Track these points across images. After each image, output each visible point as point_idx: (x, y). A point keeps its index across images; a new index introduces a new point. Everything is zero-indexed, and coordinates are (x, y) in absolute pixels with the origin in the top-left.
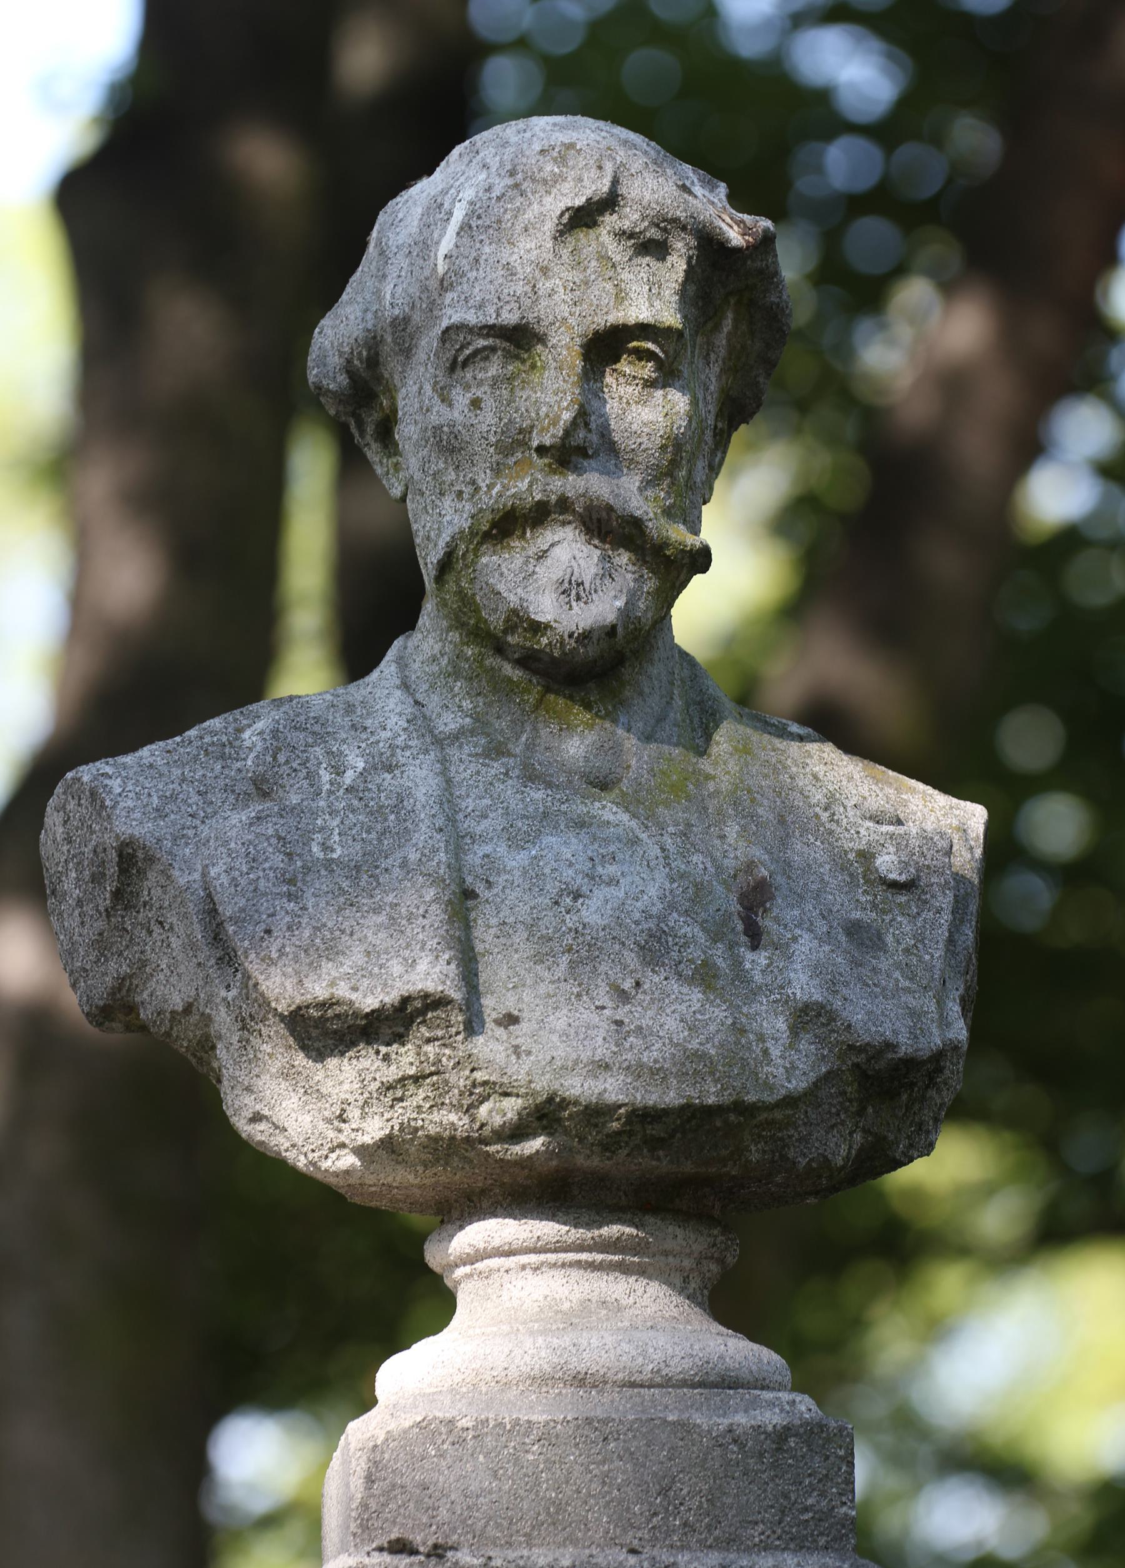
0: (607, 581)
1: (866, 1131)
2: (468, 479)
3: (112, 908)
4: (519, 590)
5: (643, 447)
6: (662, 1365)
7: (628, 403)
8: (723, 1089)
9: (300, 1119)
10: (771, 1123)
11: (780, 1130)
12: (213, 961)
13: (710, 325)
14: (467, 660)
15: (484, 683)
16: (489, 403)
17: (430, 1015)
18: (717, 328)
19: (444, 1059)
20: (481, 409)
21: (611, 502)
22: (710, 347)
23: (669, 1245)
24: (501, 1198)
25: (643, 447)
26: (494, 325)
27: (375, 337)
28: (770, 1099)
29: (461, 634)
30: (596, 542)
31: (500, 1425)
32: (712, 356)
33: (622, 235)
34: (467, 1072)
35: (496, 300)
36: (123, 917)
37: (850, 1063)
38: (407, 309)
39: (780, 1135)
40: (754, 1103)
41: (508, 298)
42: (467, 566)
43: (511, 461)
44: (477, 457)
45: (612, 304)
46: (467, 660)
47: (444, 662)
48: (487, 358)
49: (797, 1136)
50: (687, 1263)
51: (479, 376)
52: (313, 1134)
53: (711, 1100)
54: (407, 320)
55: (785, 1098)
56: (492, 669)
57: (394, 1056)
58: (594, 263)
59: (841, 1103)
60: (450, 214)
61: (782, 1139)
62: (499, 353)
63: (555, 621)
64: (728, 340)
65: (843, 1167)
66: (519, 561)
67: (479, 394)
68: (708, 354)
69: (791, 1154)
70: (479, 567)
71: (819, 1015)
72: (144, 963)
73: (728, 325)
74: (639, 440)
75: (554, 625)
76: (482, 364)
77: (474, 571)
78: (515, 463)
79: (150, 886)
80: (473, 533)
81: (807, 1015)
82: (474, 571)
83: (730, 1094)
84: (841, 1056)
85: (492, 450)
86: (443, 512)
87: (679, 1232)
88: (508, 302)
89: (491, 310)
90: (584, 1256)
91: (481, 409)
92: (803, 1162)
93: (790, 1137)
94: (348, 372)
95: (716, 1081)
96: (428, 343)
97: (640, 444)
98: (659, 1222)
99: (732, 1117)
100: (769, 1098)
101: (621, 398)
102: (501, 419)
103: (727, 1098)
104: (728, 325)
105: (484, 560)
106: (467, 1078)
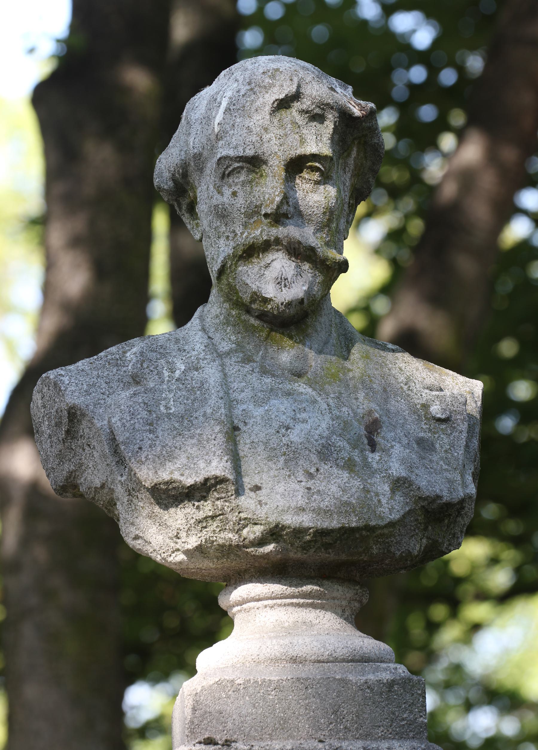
0: (299, 277)
1: (428, 538)
2: (231, 230)
3: (65, 438)
4: (257, 283)
5: (315, 213)
6: (333, 652)
7: (307, 192)
8: (359, 519)
9: (157, 538)
10: (382, 535)
11: (387, 538)
12: (114, 463)
13: (345, 154)
14: (233, 316)
15: (241, 327)
16: (241, 194)
17: (218, 487)
18: (349, 155)
19: (226, 508)
20: (237, 196)
21: (300, 240)
22: (346, 165)
23: (335, 594)
24: (254, 574)
25: (315, 213)
26: (242, 156)
27: (185, 163)
28: (382, 524)
29: (230, 304)
30: (293, 259)
31: (256, 682)
32: (347, 169)
33: (302, 112)
34: (237, 514)
35: (243, 144)
36: (71, 443)
37: (420, 505)
38: (200, 149)
39: (387, 540)
40: (374, 526)
41: (249, 143)
42: (232, 272)
43: (252, 221)
44: (235, 220)
45: (298, 145)
46: (233, 316)
47: (222, 317)
48: (239, 172)
49: (395, 541)
50: (344, 603)
51: (236, 181)
52: (164, 544)
53: (354, 525)
54: (200, 154)
55: (389, 523)
56: (245, 320)
57: (201, 507)
58: (289, 126)
59: (416, 525)
60: (220, 103)
61: (388, 543)
62: (245, 169)
63: (275, 297)
64: (355, 161)
65: (417, 556)
66: (256, 269)
67: (236, 189)
68: (345, 168)
69: (393, 549)
70: (237, 272)
71: (405, 483)
72: (81, 465)
73: (354, 154)
74: (313, 210)
75: (274, 299)
76: (237, 175)
77: (235, 274)
78: (254, 222)
79: (84, 428)
80: (234, 256)
81: (399, 483)
82: (235, 274)
83: (363, 522)
84: (416, 502)
85: (242, 216)
86: (220, 246)
87: (340, 588)
88: (249, 145)
89: (241, 149)
90: (295, 601)
91: (237, 196)
92: (398, 553)
93: (392, 541)
94: (173, 180)
95: (356, 516)
96: (211, 165)
97: (313, 212)
98: (330, 584)
99: (364, 533)
100: (381, 523)
101: (304, 190)
102: (246, 201)
103: (361, 524)
104: (354, 154)
105: (240, 269)
106: (237, 516)
